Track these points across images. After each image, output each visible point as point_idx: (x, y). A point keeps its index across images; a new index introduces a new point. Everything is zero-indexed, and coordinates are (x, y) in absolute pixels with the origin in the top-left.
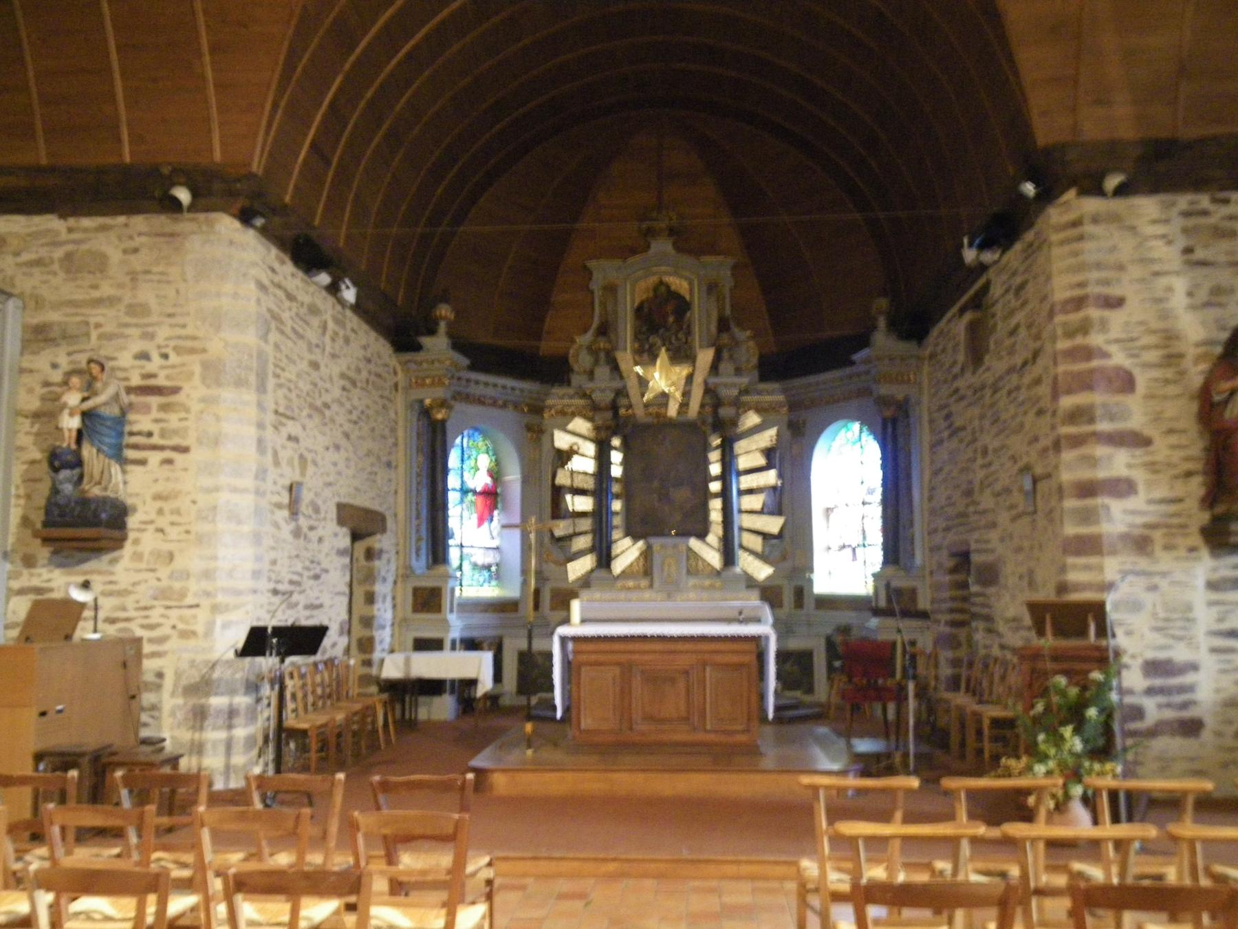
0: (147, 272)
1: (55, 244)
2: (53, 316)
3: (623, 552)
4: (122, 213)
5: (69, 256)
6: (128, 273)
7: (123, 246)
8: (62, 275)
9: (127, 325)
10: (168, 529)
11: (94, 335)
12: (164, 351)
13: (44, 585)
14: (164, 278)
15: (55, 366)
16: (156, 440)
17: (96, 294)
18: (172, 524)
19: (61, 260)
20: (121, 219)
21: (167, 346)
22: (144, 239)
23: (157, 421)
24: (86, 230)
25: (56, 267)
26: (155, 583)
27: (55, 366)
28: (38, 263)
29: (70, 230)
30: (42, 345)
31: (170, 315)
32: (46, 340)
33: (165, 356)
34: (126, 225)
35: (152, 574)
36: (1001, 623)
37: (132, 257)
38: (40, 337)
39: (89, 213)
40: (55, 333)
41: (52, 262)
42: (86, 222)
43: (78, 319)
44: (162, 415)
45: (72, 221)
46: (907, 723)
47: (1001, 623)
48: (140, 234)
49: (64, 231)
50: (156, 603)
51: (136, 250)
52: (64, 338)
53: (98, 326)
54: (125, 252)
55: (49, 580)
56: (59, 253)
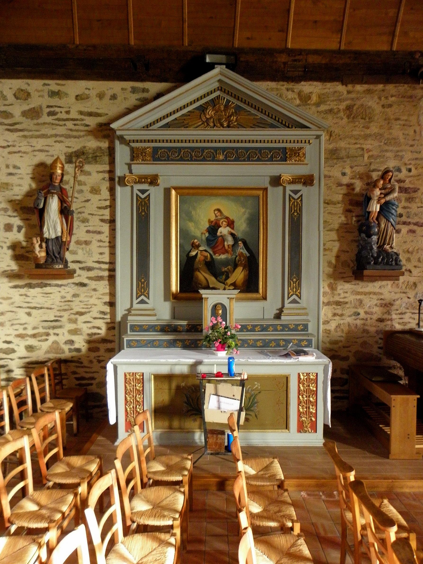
0: (397, 119)
1: (341, 101)
2: (342, 144)
3: (242, 271)
4: (381, 83)
5: (349, 108)
6: (385, 120)
7: (382, 103)
8: (345, 120)
9: (387, 151)
10: (413, 270)
11: (366, 156)
12: (409, 167)
13: (342, 300)
14: (407, 123)
15: (344, 174)
16: (404, 219)
17: (368, 132)
18: (415, 267)
19: (344, 110)
20: (381, 86)
21: (410, 164)
22: (394, 99)
23: (404, 208)
24: (358, 92)
25: (342, 114)
26: (406, 300)
27: (344, 174)
28: (331, 111)
29: (349, 92)
30: (335, 161)
31: (412, 146)
32: (338, 159)
33: (410, 170)
34: (383, 90)
35: (404, 295)
36: (383, 316)
37: (388, 110)
38: (334, 157)
39: (361, 82)
40: (343, 153)
41: (339, 111)
42: (358, 87)
43: (358, 146)
44: (407, 204)
45: (350, 87)
46: (145, 359)
47: (383, 316)
48: (392, 96)
49: (345, 92)
50: (407, 311)
51: (390, 106)
52: (348, 157)
53: (368, 151)
54: (383, 106)
55: (345, 298)
56: (343, 106)
